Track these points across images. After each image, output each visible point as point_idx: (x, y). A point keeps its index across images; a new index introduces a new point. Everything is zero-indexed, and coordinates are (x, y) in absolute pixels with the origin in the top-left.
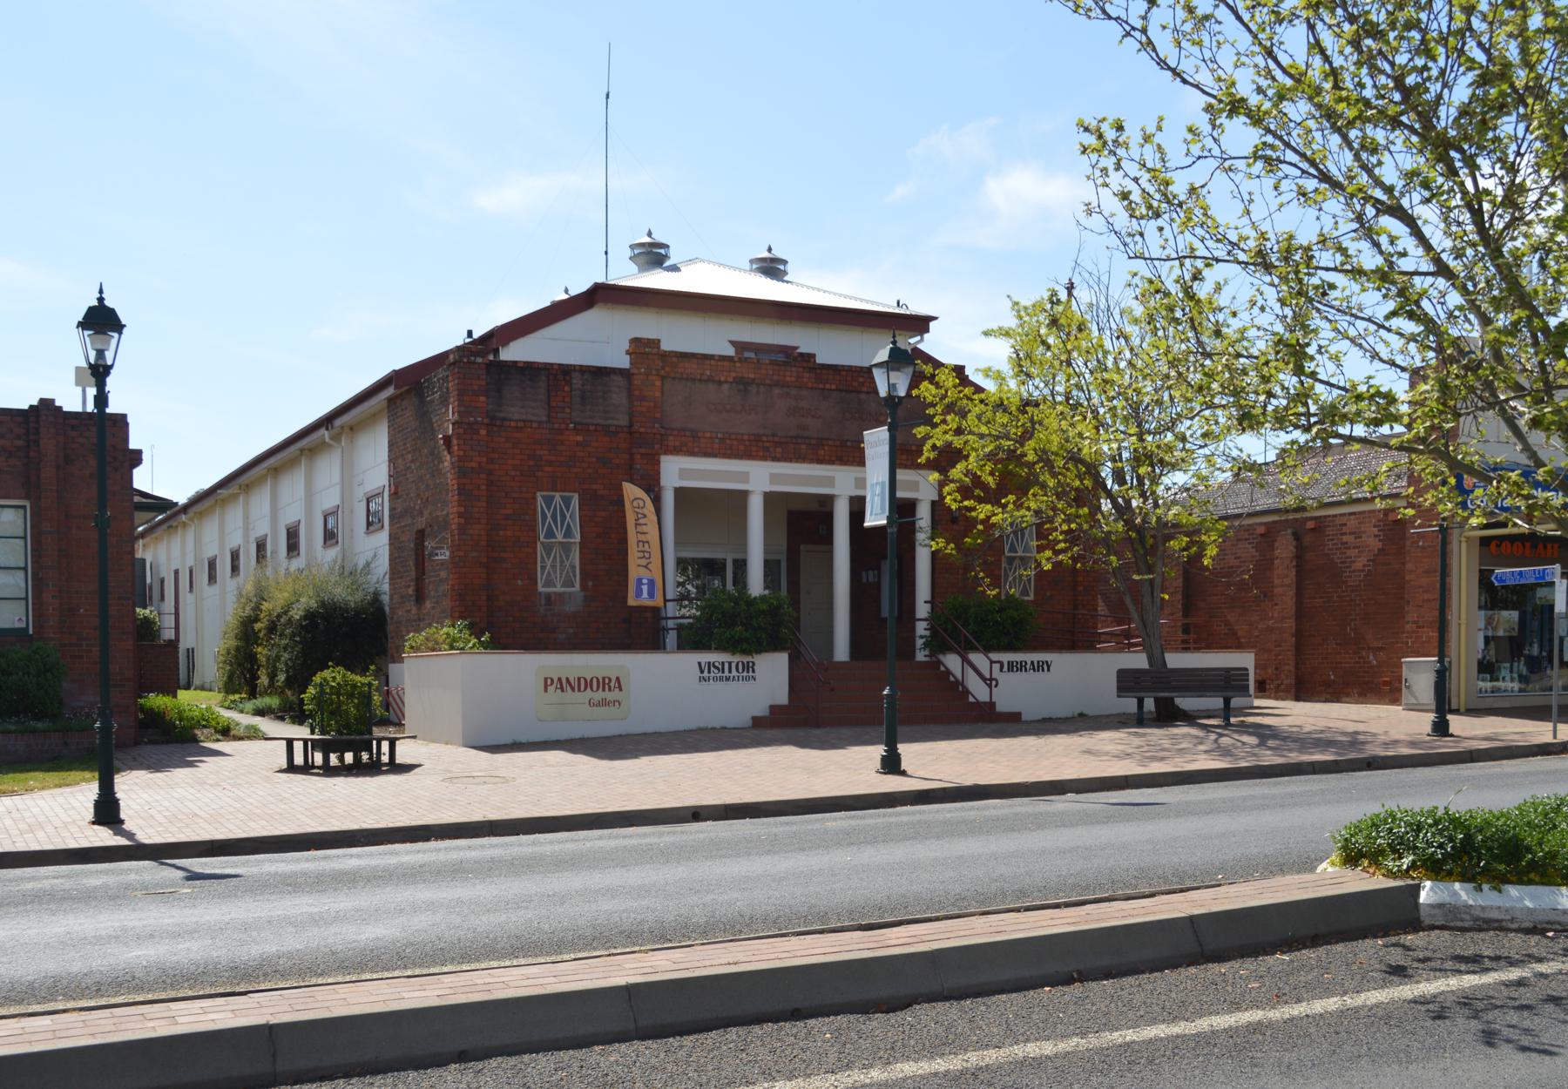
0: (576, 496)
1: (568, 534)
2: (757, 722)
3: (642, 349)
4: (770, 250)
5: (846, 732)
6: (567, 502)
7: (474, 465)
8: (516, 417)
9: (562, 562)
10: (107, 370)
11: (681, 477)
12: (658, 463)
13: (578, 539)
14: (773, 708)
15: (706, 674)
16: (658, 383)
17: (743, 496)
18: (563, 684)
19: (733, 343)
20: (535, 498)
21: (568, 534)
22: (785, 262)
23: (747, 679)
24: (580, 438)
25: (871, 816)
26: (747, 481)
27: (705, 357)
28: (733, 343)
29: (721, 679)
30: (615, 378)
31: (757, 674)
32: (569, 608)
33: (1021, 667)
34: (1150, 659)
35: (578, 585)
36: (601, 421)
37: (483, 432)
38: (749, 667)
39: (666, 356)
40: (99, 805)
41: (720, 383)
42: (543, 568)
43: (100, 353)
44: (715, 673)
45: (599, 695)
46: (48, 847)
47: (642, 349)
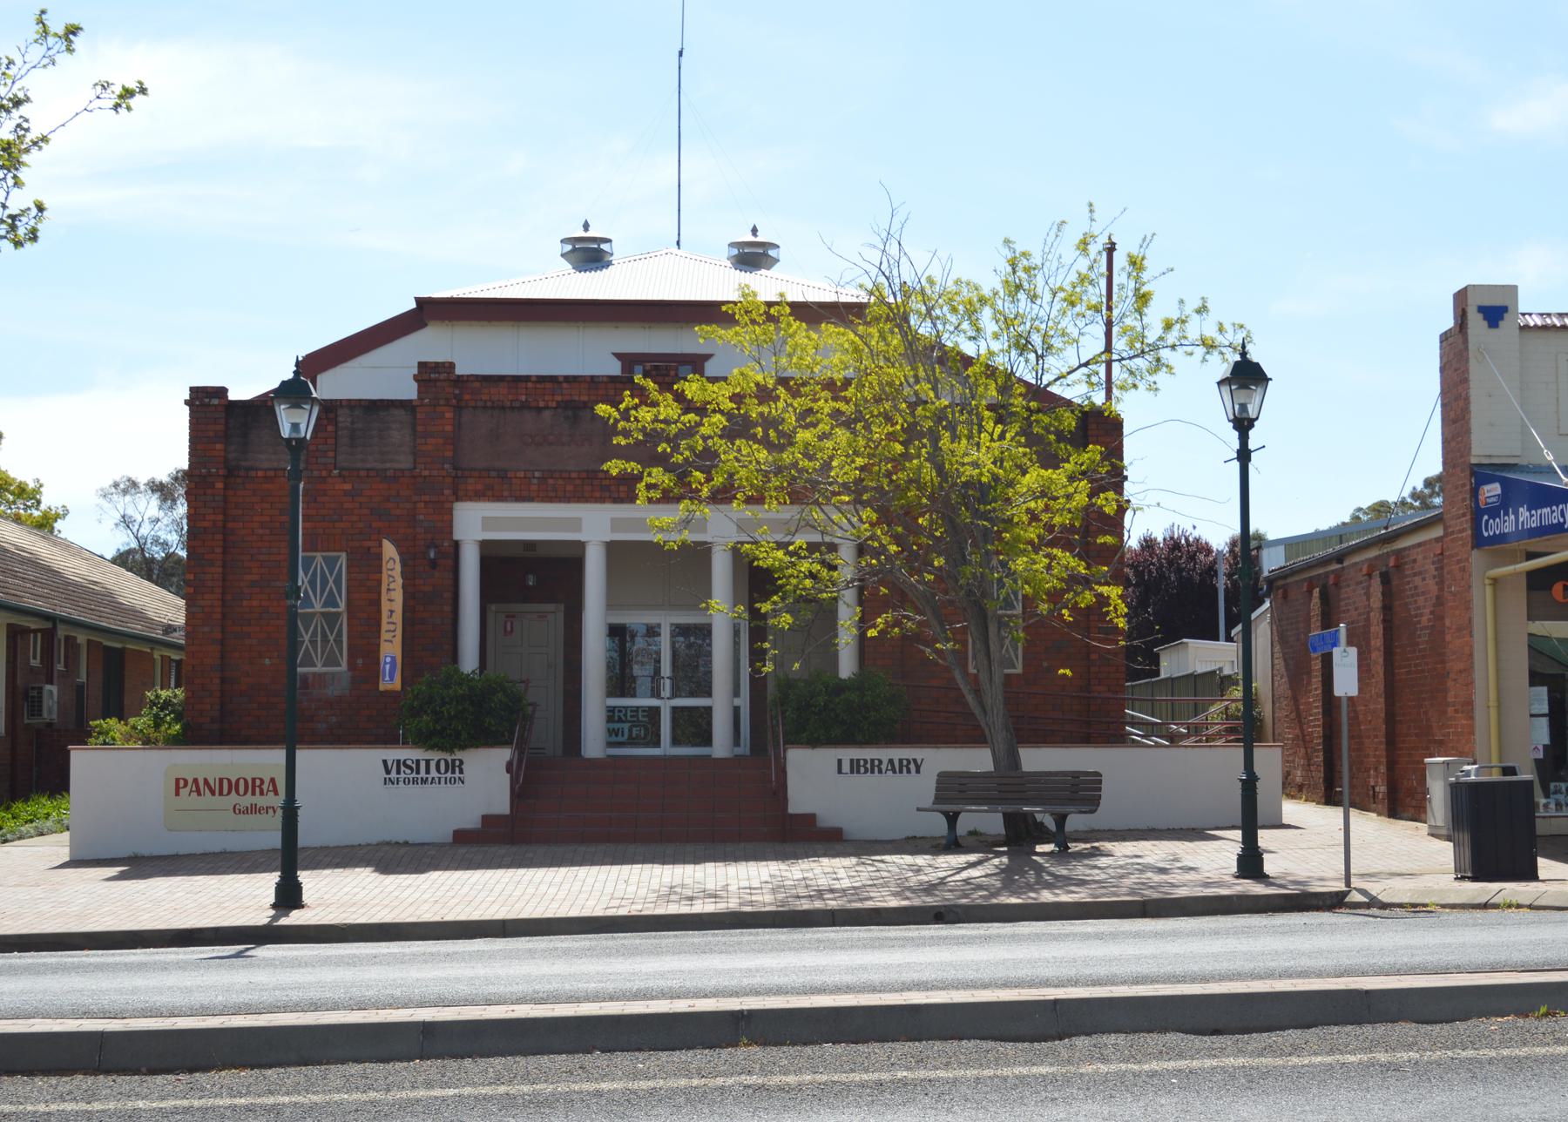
0: (344, 555)
1: (331, 601)
2: (461, 837)
3: (431, 375)
4: (754, 231)
5: (500, 850)
6: (331, 563)
7: (206, 524)
8: (266, 465)
9: (324, 635)
10: (1251, 423)
11: (614, 529)
12: (451, 511)
14: (487, 819)
15: (393, 775)
16: (449, 415)
18: (199, 787)
19: (618, 356)
21: (331, 601)
22: (609, 241)
23: (452, 781)
24: (347, 487)
25: (1237, 933)
26: (579, 529)
27: (517, 380)
28: (618, 356)
29: (415, 781)
30: (396, 412)
31: (467, 775)
32: (332, 691)
33: (873, 767)
34: (1015, 763)
35: (344, 666)
36: (379, 466)
37: (220, 485)
38: (455, 767)
40: (1241, 860)
41: (539, 410)
43: (1243, 407)
44: (405, 773)
45: (247, 800)
46: (562, 913)
47: (431, 375)
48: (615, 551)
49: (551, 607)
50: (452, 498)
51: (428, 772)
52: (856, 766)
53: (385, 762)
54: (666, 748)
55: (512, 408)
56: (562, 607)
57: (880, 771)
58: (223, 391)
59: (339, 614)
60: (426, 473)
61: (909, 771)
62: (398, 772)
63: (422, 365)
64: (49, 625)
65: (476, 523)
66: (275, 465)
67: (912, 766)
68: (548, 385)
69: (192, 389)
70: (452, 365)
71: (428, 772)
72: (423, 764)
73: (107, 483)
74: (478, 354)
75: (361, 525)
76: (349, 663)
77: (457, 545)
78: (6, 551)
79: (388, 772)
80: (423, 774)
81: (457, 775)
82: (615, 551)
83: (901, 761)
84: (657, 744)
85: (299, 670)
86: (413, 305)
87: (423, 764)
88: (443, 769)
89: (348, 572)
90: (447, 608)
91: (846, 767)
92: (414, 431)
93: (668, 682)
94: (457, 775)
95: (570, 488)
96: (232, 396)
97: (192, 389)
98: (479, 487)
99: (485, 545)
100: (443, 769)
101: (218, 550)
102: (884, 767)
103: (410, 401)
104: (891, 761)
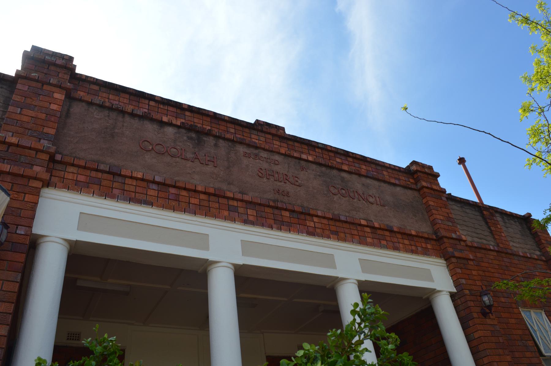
48: (247, 280)
95: (196, 201)
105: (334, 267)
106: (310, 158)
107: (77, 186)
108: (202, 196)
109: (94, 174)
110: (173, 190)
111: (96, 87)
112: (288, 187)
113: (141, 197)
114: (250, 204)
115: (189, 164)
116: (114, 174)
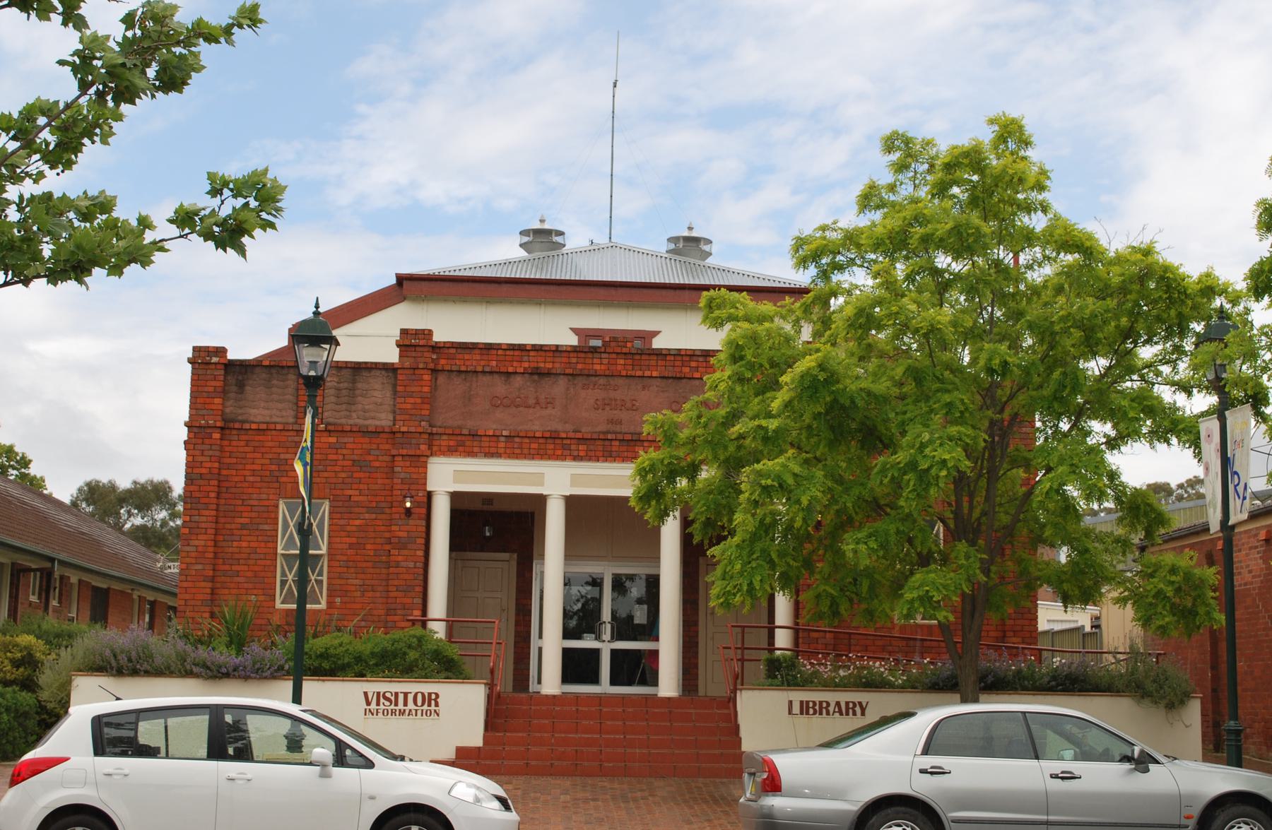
11: (573, 484)
13: (324, 550)
15: (373, 706)
17: (541, 500)
19: (576, 331)
20: (277, 506)
22: (561, 233)
27: (489, 348)
28: (576, 331)
29: (393, 712)
31: (441, 709)
37: (217, 436)
39: (438, 348)
42: (283, 583)
47: (412, 341)
48: (574, 504)
49: (505, 556)
50: (428, 453)
51: (405, 704)
52: (805, 708)
53: (366, 694)
54: (605, 686)
55: (483, 372)
56: (515, 556)
57: (828, 713)
58: (221, 351)
59: (321, 556)
60: (404, 429)
61: (854, 714)
62: (378, 704)
63: (404, 332)
64: (48, 565)
65: (448, 476)
66: (268, 419)
67: (858, 709)
68: (517, 353)
69: (195, 349)
70: (430, 333)
71: (405, 704)
72: (401, 697)
73: (992, 115)
74: (453, 325)
75: (344, 475)
76: (328, 602)
77: (430, 495)
78: (10, 502)
79: (368, 703)
80: (401, 706)
81: (433, 707)
82: (574, 504)
83: (847, 703)
84: (595, 680)
85: (308, 606)
86: (393, 281)
87: (401, 697)
88: (419, 702)
89: (330, 519)
90: (420, 553)
91: (796, 709)
92: (395, 392)
93: (609, 626)
94: (433, 707)
95: (535, 446)
96: (231, 356)
97: (195, 349)
98: (452, 443)
99: (455, 497)
100: (419, 702)
101: (213, 495)
102: (831, 709)
103: (393, 364)
104: (838, 704)
105: (542, 485)
106: (655, 374)
107: (451, 451)
108: (541, 441)
109: (459, 438)
110: (517, 440)
111: (453, 351)
112: (617, 414)
113: (492, 450)
114: (583, 440)
115: (531, 410)
116: (473, 435)
